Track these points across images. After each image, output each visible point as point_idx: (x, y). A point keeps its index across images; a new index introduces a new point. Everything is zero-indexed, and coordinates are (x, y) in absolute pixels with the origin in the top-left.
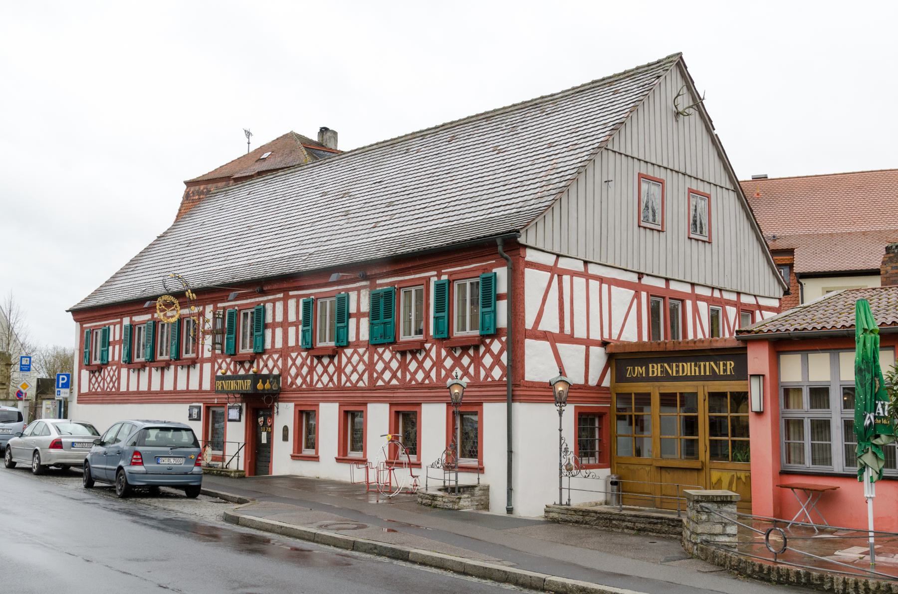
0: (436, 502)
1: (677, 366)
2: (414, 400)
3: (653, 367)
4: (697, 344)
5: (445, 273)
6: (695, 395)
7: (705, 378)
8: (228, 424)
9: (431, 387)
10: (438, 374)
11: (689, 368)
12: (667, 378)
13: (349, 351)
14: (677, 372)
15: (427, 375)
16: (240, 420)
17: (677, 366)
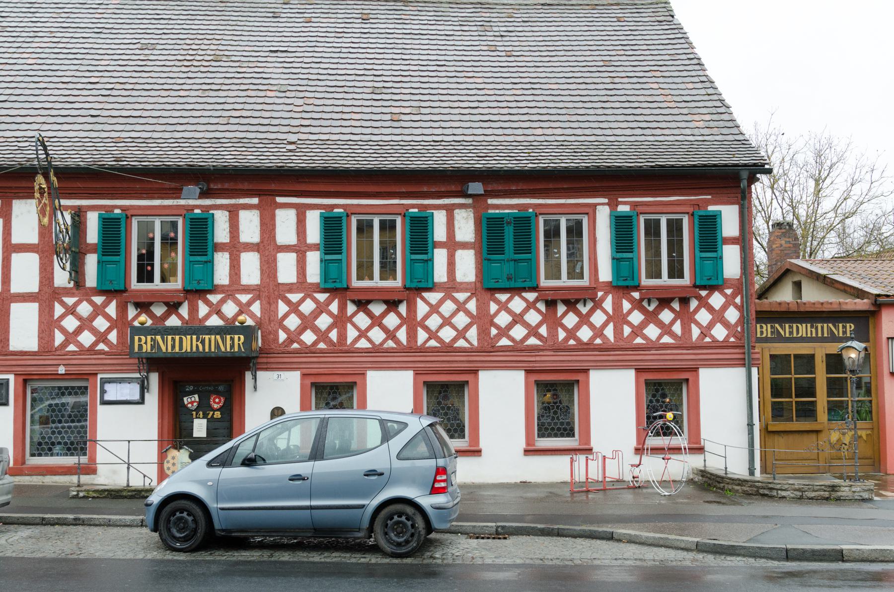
0: (839, 494)
1: (791, 327)
2: (577, 366)
3: (762, 327)
4: (825, 306)
5: (625, 203)
6: (812, 357)
7: (823, 340)
8: (102, 410)
9: (606, 349)
10: (618, 332)
11: (804, 329)
12: (780, 339)
13: (433, 297)
14: (791, 333)
15: (599, 332)
16: (142, 401)
17: (791, 327)
